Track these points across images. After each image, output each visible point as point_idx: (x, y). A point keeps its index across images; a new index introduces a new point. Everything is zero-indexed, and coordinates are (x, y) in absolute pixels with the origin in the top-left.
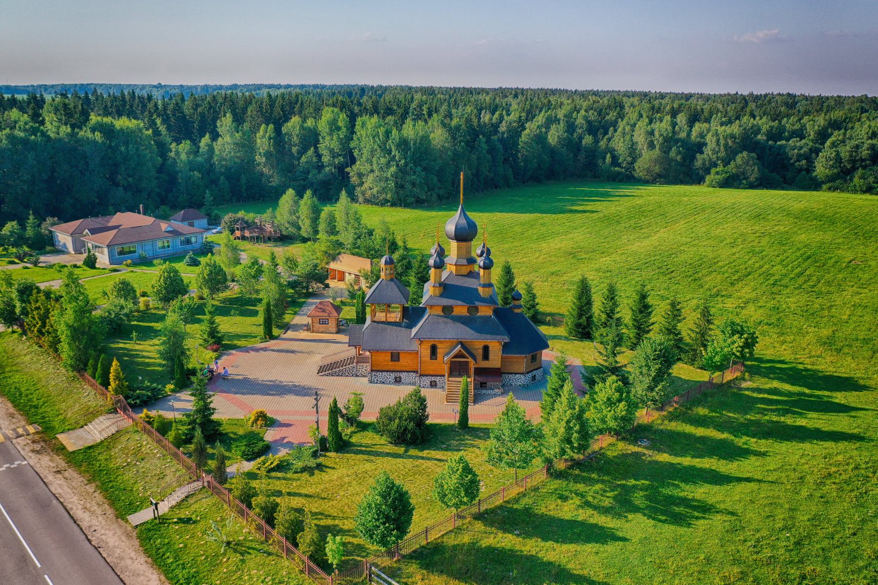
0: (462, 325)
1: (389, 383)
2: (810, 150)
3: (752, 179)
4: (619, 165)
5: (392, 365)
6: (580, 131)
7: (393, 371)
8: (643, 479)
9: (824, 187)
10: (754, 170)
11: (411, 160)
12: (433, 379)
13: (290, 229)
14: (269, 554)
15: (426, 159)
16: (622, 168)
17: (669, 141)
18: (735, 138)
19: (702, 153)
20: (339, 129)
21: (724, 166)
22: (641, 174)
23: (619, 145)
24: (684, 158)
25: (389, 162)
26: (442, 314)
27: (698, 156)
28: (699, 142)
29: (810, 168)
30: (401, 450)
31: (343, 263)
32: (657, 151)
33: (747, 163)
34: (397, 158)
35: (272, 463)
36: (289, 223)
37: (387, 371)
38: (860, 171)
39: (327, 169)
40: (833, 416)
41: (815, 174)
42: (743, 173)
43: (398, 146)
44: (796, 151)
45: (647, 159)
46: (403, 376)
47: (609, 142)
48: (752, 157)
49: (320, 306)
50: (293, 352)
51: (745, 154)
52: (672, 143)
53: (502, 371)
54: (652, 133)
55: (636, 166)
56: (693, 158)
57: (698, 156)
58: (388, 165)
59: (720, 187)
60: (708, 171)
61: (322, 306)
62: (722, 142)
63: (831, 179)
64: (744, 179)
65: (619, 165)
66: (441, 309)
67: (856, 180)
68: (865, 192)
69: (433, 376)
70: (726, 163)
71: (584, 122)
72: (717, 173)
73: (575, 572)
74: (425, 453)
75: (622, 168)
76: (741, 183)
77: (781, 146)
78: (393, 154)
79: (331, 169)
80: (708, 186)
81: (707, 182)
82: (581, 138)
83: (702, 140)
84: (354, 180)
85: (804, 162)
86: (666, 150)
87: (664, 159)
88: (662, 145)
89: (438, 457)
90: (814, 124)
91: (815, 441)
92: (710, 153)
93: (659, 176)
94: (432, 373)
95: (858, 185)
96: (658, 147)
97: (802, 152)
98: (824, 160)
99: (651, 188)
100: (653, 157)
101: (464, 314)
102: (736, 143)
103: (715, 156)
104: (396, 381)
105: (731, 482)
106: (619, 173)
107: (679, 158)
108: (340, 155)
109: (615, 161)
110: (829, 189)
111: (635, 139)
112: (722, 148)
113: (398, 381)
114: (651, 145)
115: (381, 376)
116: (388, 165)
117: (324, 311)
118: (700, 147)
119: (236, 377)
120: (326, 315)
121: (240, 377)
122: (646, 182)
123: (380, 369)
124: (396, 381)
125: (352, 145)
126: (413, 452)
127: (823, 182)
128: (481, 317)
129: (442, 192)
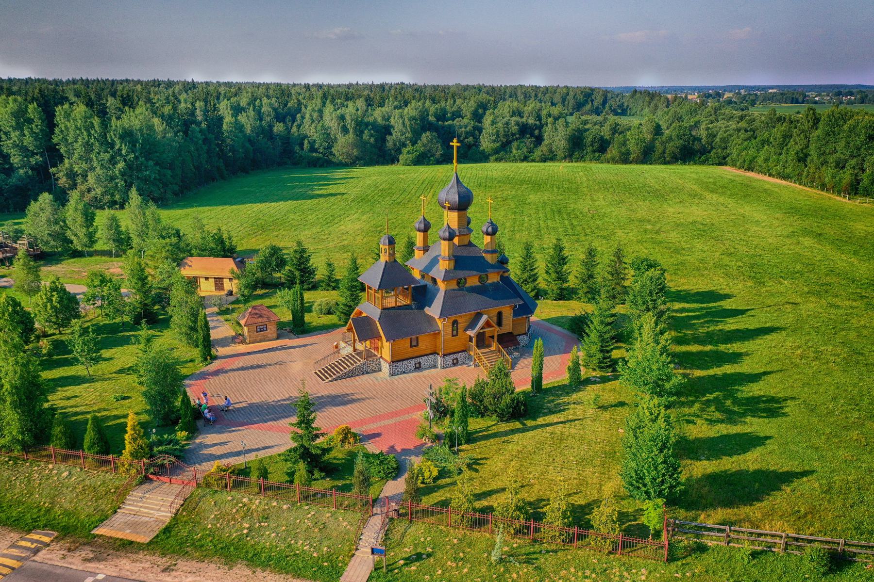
0: (479, 296)
1: (410, 372)
2: (473, 127)
3: (438, 155)
4: (316, 151)
5: (411, 352)
6: (269, 119)
7: (413, 358)
8: (715, 392)
9: (492, 158)
10: (438, 147)
11: (141, 153)
12: (455, 356)
13: (52, 243)
14: (556, 551)
15: (156, 152)
16: (319, 153)
17: (361, 126)
18: (416, 120)
19: (391, 134)
20: (30, 121)
21: (413, 146)
22: (340, 158)
23: (310, 130)
24: (376, 140)
25: (113, 158)
26: (457, 287)
27: (388, 137)
28: (385, 125)
29: (477, 143)
30: (517, 425)
31: (194, 267)
32: (351, 136)
33: (431, 141)
34: (124, 152)
35: (51, 560)
36: (50, 235)
37: (407, 359)
38: (515, 144)
39: (22, 171)
40: (739, 318)
41: (481, 148)
42: (429, 151)
43: (122, 138)
44: (463, 129)
45: (343, 144)
46: (423, 360)
47: (299, 129)
48: (434, 136)
49: (254, 312)
50: (259, 366)
51: (428, 133)
52: (363, 127)
53: (515, 333)
54: (342, 118)
55: (334, 150)
56: (384, 140)
57: (388, 137)
58: (113, 161)
59: (414, 165)
60: (399, 151)
61: (257, 311)
62: (408, 123)
63: (496, 152)
64: (431, 156)
65: (316, 151)
66: (455, 282)
67: (514, 151)
68: (523, 161)
69: (454, 353)
70: (414, 143)
71: (270, 109)
72: (409, 152)
73: (781, 471)
74: (540, 421)
75: (319, 153)
76: (430, 160)
77: (450, 126)
78: (117, 147)
79: (26, 172)
80: (403, 165)
81: (401, 161)
82: (271, 127)
83: (387, 123)
84: (63, 181)
85: (471, 138)
86: (359, 133)
87: (360, 144)
88: (355, 129)
89: (556, 420)
90: (468, 107)
91: (760, 337)
92: (399, 134)
93: (358, 158)
94: (453, 351)
95: (517, 155)
96: (351, 131)
97: (468, 129)
98: (488, 135)
99: (356, 171)
100: (351, 140)
101: (476, 284)
102: (417, 124)
103: (403, 137)
104: (416, 368)
105: (761, 378)
106: (319, 159)
107: (372, 140)
108: (37, 154)
109: (313, 149)
110: (496, 160)
111: (327, 124)
112: (409, 129)
113: (418, 368)
114: (345, 130)
115: (402, 366)
116: (113, 161)
117: (261, 316)
118: (387, 130)
119: (238, 406)
120: (265, 320)
121: (244, 405)
122: (345, 165)
123: (400, 358)
124: (416, 368)
125: (55, 140)
126: (529, 423)
127: (489, 155)
128: (491, 284)
129: (176, 188)
